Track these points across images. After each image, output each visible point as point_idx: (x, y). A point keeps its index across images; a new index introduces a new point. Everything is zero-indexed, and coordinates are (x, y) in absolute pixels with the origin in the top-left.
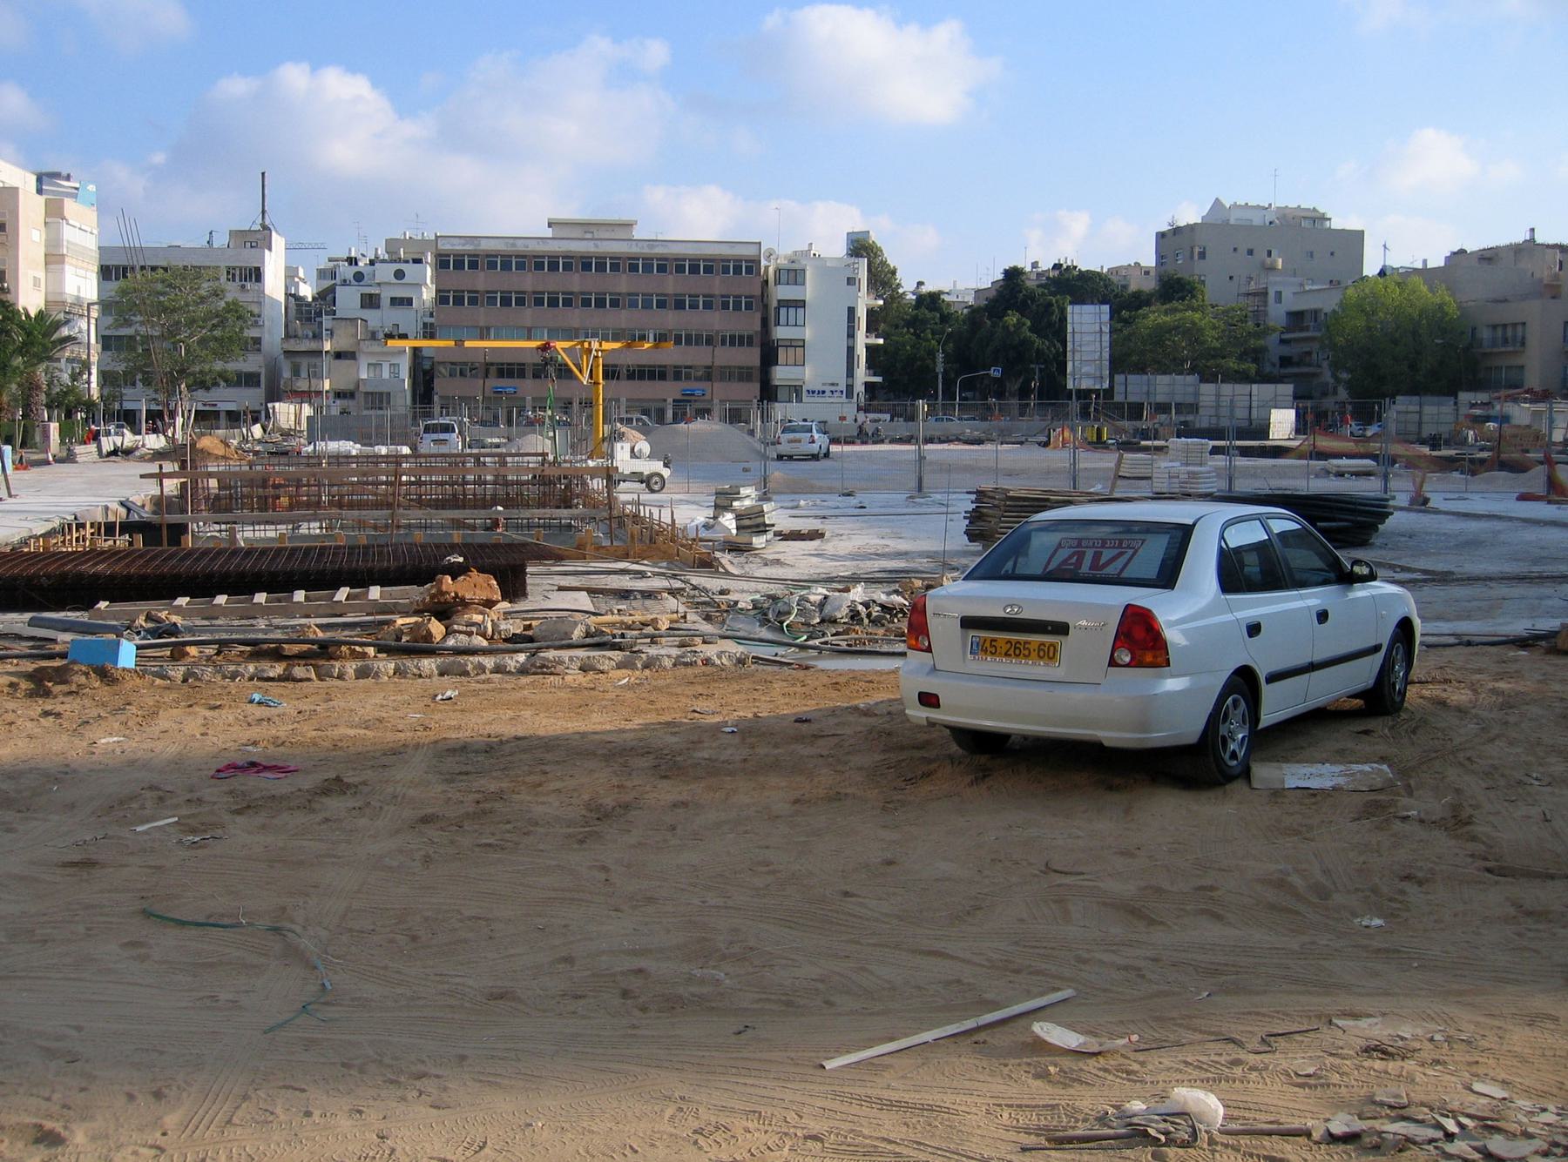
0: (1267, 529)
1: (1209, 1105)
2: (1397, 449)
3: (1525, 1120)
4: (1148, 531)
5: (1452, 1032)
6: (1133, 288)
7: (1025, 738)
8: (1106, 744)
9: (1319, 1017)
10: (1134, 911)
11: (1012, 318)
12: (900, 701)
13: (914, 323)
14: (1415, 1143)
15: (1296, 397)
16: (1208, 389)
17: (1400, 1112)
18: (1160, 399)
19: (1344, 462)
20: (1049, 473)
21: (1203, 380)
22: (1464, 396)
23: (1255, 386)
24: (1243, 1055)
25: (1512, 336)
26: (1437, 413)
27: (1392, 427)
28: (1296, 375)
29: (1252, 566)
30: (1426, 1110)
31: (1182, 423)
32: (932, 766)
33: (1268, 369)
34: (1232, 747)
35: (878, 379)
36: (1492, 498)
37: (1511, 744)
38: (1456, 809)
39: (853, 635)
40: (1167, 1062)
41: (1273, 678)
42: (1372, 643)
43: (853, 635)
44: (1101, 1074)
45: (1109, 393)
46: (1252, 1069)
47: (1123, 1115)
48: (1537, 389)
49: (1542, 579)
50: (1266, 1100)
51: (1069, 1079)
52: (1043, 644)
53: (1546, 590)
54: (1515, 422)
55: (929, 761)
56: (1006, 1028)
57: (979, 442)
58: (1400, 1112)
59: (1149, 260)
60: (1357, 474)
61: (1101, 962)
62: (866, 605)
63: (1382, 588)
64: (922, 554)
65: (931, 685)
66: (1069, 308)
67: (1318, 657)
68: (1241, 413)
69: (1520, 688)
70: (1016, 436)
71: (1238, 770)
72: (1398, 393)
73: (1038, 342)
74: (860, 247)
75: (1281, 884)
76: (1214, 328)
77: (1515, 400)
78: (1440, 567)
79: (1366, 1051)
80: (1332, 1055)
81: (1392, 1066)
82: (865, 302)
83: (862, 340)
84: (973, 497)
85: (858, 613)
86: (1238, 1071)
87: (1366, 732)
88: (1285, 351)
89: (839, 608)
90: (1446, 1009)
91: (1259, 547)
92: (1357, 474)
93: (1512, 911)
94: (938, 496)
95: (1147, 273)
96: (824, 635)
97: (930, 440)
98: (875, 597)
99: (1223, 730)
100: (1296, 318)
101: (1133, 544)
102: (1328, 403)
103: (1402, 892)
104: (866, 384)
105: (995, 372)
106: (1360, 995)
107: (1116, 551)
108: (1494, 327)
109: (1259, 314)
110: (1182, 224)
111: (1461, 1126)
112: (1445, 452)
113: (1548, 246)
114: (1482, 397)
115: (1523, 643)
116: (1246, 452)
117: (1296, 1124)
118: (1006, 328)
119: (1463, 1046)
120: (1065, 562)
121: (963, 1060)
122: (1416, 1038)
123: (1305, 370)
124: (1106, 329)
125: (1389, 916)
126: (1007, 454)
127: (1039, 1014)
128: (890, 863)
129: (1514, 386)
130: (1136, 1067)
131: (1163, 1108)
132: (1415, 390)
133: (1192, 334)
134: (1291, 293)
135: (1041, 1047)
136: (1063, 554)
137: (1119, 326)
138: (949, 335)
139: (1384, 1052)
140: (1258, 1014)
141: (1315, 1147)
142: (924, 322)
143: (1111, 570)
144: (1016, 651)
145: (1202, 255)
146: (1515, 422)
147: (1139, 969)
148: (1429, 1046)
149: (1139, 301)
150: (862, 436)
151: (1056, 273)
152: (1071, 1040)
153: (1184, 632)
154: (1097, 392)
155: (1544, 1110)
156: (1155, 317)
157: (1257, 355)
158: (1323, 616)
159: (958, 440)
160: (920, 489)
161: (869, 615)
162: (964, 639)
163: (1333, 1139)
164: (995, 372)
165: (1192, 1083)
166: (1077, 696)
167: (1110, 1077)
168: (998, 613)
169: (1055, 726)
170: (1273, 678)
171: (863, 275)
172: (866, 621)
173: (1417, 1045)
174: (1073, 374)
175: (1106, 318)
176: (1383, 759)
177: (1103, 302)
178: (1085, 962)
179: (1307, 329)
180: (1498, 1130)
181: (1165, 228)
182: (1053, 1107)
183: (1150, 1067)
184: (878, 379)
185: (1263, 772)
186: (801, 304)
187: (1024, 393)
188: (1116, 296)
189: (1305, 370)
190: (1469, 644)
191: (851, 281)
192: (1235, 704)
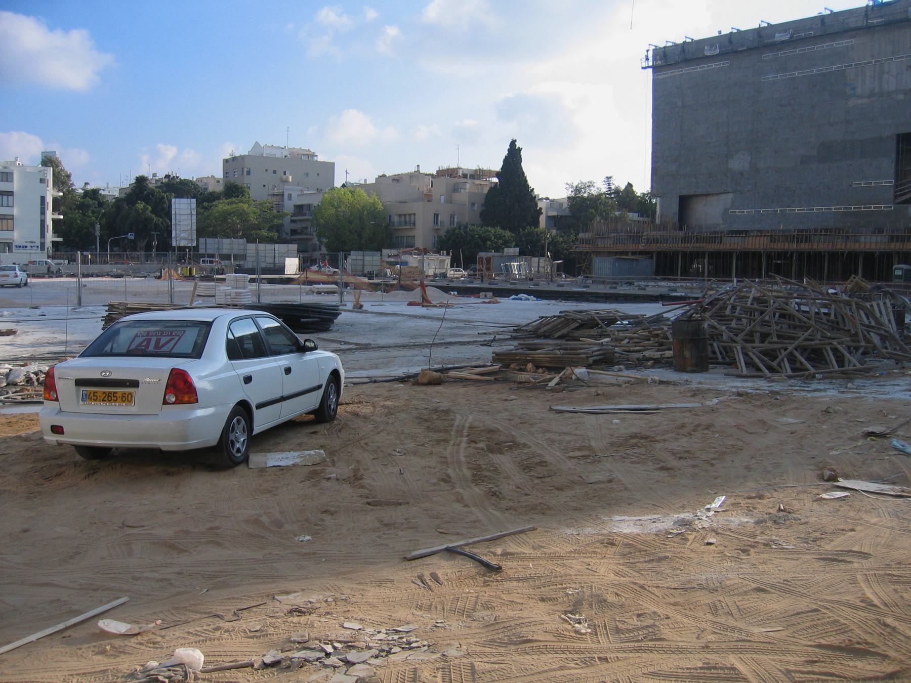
0: (257, 325)
1: (195, 656)
2: (351, 279)
3: (368, 639)
4: (187, 326)
5: (338, 595)
6: (210, 189)
7: (117, 449)
8: (163, 449)
9: (268, 596)
10: (171, 546)
11: (140, 205)
12: (41, 432)
13: (82, 207)
14: (309, 662)
15: (299, 251)
16: (251, 246)
17: (303, 645)
18: (225, 252)
19: (322, 286)
20: (158, 294)
21: (250, 241)
22: (386, 252)
23: (277, 245)
24: (222, 624)
25: (409, 220)
26: (371, 260)
27: (349, 268)
28: (299, 239)
29: (249, 345)
30: (317, 642)
31: (237, 265)
32: (63, 469)
33: (284, 236)
34: (238, 446)
35: (60, 239)
36: (396, 305)
37: (388, 434)
38: (356, 471)
39: (26, 392)
40: (177, 634)
41: (260, 406)
42: (317, 384)
43: (26, 392)
44: (138, 646)
45: (196, 248)
46: (226, 631)
47: (145, 670)
48: (421, 247)
49: (415, 346)
50: (231, 649)
51: (119, 652)
52: (125, 393)
53: (416, 352)
54: (410, 265)
55: (61, 466)
56: (85, 626)
57: (120, 276)
58: (303, 645)
59: (220, 175)
60: (328, 293)
61: (147, 578)
62: (36, 374)
63: (321, 354)
64: (76, 342)
65: (58, 421)
66: (173, 200)
67: (286, 393)
68: (270, 260)
69: (397, 404)
70: (143, 273)
71: (242, 458)
72: (352, 250)
73: (155, 219)
74: (49, 161)
75: (256, 522)
76: (255, 213)
77: (411, 254)
78: (364, 341)
79: (290, 612)
80: (271, 617)
81: (303, 619)
82: (51, 193)
83: (50, 216)
84: (107, 308)
85: (31, 379)
86: (218, 634)
87: (315, 433)
88: (294, 226)
89: (18, 377)
90: (336, 583)
91: (253, 336)
92: (328, 293)
93: (377, 525)
94: (91, 308)
95: (218, 182)
96: (8, 393)
97: (85, 276)
98: (42, 369)
99: (232, 437)
100: (299, 208)
101: (178, 333)
102: (317, 255)
103: (322, 520)
104: (53, 242)
105: (131, 236)
106: (292, 580)
107: (169, 338)
108: (400, 215)
109: (280, 206)
110: (237, 155)
111: (335, 648)
112: (376, 281)
113: (426, 175)
114: (394, 252)
115: (402, 380)
116: (271, 281)
117: (246, 660)
118: (137, 211)
119: (343, 603)
120: (140, 345)
121: (54, 649)
122: (318, 601)
123: (304, 237)
124: (194, 212)
125: (314, 534)
126: (134, 283)
127: (107, 614)
128: (26, 531)
129: (409, 246)
130: (159, 639)
131: (169, 663)
132: (360, 248)
133: (242, 215)
134: (297, 195)
135: (105, 635)
136: (139, 340)
137: (202, 211)
138: (104, 214)
139: (299, 612)
140: (233, 598)
141: (255, 672)
142: (88, 206)
143: (165, 349)
144: (109, 398)
145: (249, 173)
146: (410, 265)
147: (169, 580)
148: (324, 604)
149: (213, 197)
150: (50, 273)
151: (167, 180)
152: (120, 627)
153: (209, 381)
154: (189, 248)
155: (379, 632)
156: (222, 206)
157: (279, 228)
158: (288, 371)
159: (108, 275)
160: (80, 304)
161: (38, 380)
162: (77, 392)
163: (266, 666)
164: (131, 236)
165: (190, 644)
166: (147, 422)
167: (143, 648)
168: (97, 376)
169: (133, 440)
170: (260, 406)
171: (50, 177)
172: (36, 383)
173: (318, 605)
174: (176, 237)
175: (194, 206)
176: (322, 447)
177: (193, 198)
178: (137, 579)
179: (305, 215)
180: (353, 647)
181: (228, 157)
182: (104, 671)
183: (167, 638)
184: (60, 239)
185: (256, 459)
186: (10, 193)
187: (148, 248)
188: (201, 194)
189: (304, 237)
190: (375, 382)
191: (42, 181)
192: (238, 422)
